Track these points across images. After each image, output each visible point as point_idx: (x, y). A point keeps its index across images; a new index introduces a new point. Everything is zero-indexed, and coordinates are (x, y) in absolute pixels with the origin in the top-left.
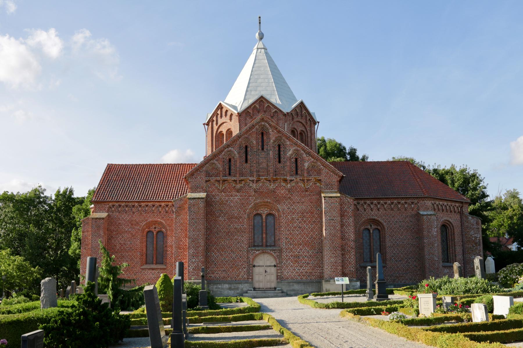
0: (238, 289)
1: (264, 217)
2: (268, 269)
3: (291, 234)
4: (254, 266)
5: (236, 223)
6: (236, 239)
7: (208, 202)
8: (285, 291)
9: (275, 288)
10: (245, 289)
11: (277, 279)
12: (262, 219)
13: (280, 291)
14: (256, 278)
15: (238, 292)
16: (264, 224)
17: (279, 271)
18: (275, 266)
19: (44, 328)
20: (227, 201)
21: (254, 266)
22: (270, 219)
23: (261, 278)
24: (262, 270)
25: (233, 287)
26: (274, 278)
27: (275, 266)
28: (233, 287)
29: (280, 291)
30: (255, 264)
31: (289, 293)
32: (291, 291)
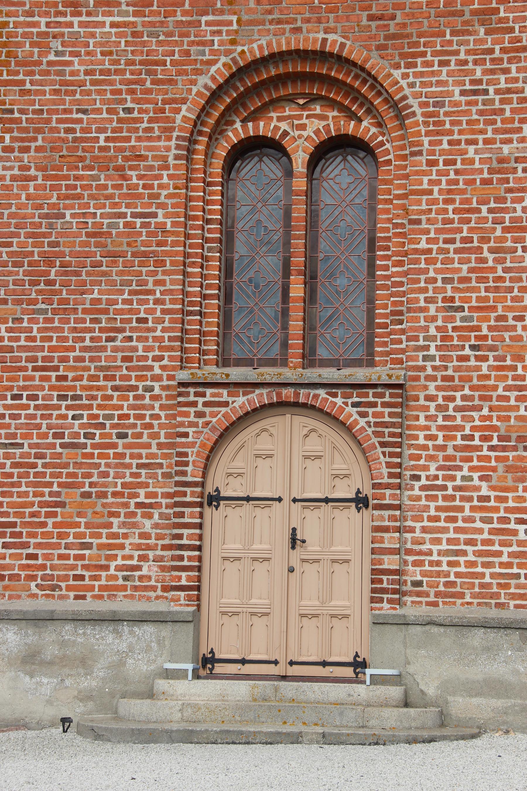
0: (84, 662)
1: (300, 160)
2: (312, 525)
3: (481, 271)
4: (215, 499)
5: (101, 195)
6: (96, 310)
7: (251, 598)
8: (431, 691)
9: (359, 664)
10: (139, 666)
11: (377, 594)
12: (289, 173)
13: (395, 692)
14: (224, 587)
15: (88, 683)
16: (299, 211)
17: (390, 540)
18: (361, 502)
19: (175, 419)
20: (42, 42)
21: (215, 499)
22: (340, 173)
23: (264, 587)
24: (267, 528)
25: (51, 651)
26: (350, 589)
27: (361, 502)
28: (51, 651)
29: (395, 692)
30: (217, 480)
31: (460, 706)
32: (475, 689)
